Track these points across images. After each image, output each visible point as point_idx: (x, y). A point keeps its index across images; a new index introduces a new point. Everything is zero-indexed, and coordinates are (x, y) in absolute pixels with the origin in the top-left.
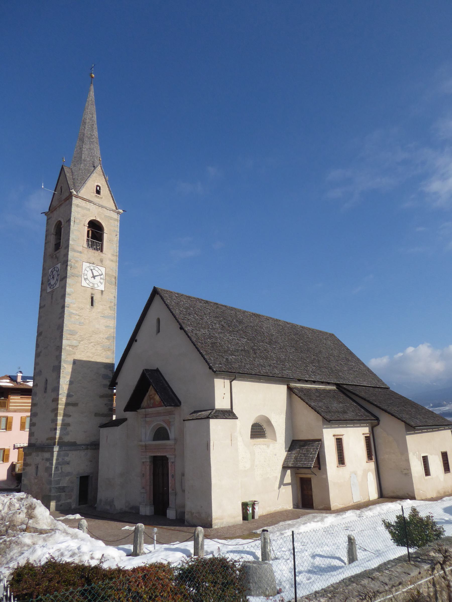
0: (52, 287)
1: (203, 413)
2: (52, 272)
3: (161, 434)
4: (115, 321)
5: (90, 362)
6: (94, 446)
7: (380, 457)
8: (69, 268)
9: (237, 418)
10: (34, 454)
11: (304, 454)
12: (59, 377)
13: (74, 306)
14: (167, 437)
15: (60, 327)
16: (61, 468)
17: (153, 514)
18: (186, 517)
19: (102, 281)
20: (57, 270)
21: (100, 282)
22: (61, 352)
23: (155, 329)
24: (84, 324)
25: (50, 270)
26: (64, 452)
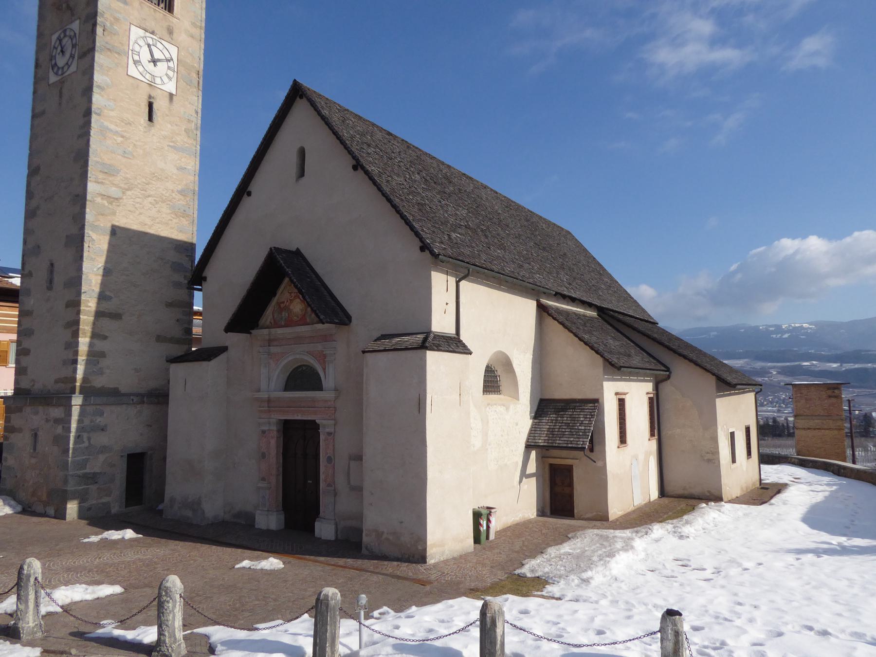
0: (60, 72)
1: (406, 338)
2: (60, 40)
3: (303, 378)
4: (198, 160)
5: (146, 234)
6: (159, 397)
7: (663, 434)
8: (99, 30)
9: (470, 353)
10: (28, 410)
11: (568, 425)
12: (81, 257)
13: (112, 114)
14: (317, 385)
15: (82, 157)
16: (89, 439)
17: (283, 527)
18: (365, 539)
19: (170, 73)
20: (72, 34)
21: (167, 75)
22: (84, 206)
23: (294, 170)
24: (134, 156)
25: (55, 37)
26: (94, 407)
